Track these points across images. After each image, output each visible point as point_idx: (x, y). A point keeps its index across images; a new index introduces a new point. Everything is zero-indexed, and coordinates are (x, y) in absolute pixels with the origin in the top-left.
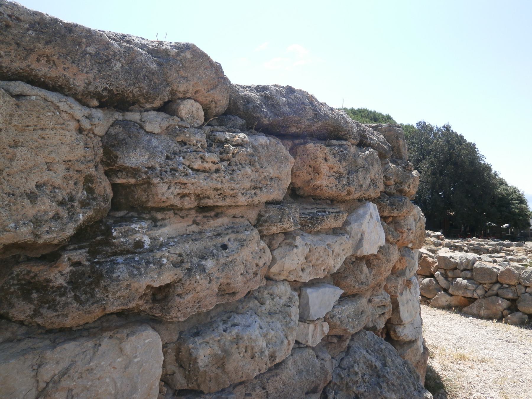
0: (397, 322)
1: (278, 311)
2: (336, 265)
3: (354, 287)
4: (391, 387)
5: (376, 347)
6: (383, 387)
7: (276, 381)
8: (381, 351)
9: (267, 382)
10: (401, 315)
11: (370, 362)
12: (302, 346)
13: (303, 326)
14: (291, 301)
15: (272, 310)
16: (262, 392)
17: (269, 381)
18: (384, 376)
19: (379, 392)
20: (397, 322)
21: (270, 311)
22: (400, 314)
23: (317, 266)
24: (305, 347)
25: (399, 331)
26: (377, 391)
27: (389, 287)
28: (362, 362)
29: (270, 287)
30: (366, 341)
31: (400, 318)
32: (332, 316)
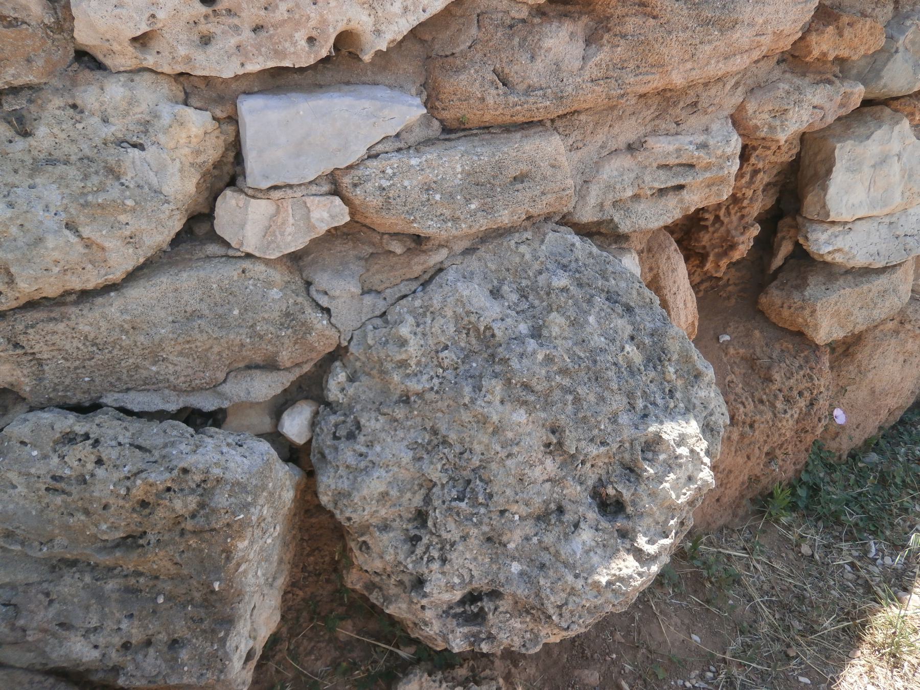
0: (818, 215)
1: (73, 158)
2: (383, 28)
3: (483, 99)
4: (519, 392)
5: (542, 280)
6: (484, 389)
7: (54, 333)
8: (548, 294)
9: (25, 333)
10: (828, 197)
11: (473, 318)
12: (231, 253)
13: (233, 202)
14: (146, 132)
15: (57, 154)
16: (11, 352)
17: (30, 331)
18: (505, 361)
19: (467, 400)
20: (818, 215)
21: (50, 154)
22: (825, 195)
23: (275, 26)
24: (240, 257)
25: (817, 240)
26: (463, 397)
27: (750, 112)
28: (449, 313)
29: (83, 88)
30: (517, 260)
31: (824, 206)
32: (356, 180)
